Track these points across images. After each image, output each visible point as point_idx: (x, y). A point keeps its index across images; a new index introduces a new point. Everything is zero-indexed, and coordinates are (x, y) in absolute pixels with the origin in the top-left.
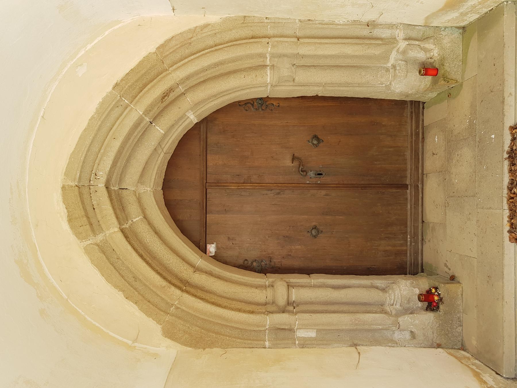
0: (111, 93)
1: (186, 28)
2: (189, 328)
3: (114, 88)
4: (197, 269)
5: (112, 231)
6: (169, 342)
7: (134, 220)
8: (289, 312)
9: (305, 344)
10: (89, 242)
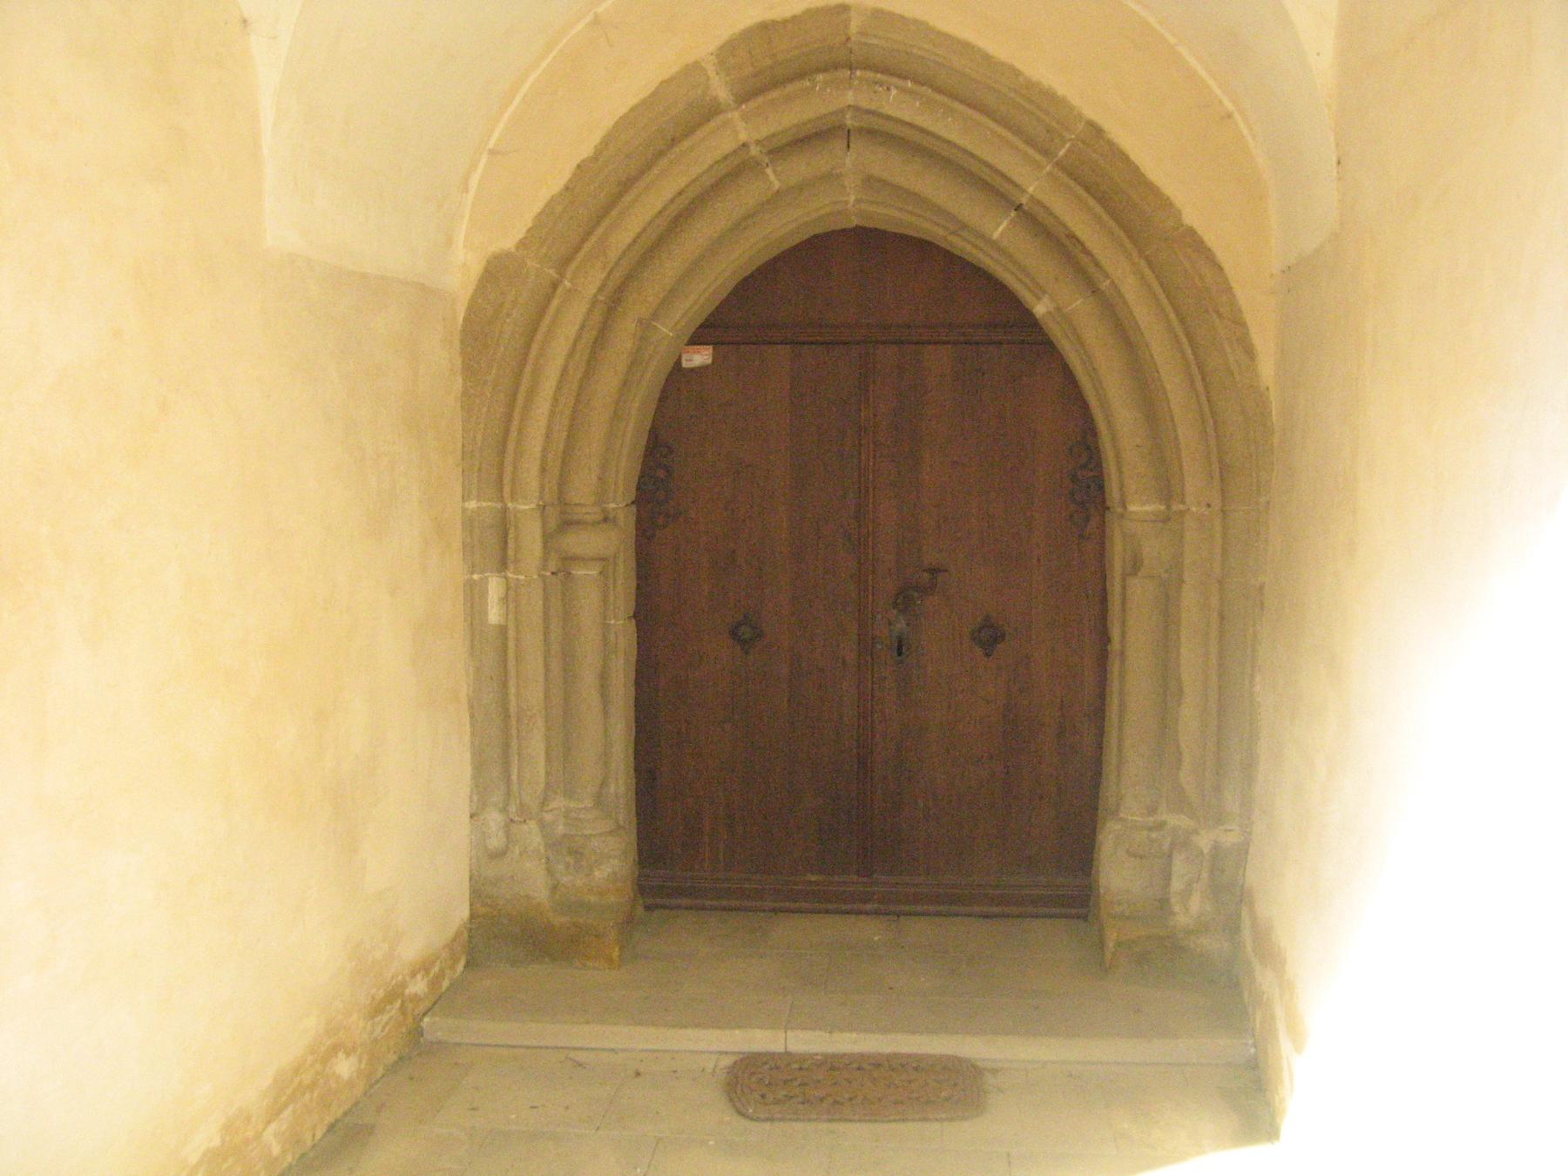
0: (1080, 115)
1: (1242, 301)
2: (508, 315)
3: (1091, 124)
4: (645, 325)
5: (741, 125)
6: (476, 269)
7: (769, 171)
8: (545, 560)
9: (474, 597)
10: (712, 74)
